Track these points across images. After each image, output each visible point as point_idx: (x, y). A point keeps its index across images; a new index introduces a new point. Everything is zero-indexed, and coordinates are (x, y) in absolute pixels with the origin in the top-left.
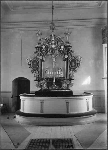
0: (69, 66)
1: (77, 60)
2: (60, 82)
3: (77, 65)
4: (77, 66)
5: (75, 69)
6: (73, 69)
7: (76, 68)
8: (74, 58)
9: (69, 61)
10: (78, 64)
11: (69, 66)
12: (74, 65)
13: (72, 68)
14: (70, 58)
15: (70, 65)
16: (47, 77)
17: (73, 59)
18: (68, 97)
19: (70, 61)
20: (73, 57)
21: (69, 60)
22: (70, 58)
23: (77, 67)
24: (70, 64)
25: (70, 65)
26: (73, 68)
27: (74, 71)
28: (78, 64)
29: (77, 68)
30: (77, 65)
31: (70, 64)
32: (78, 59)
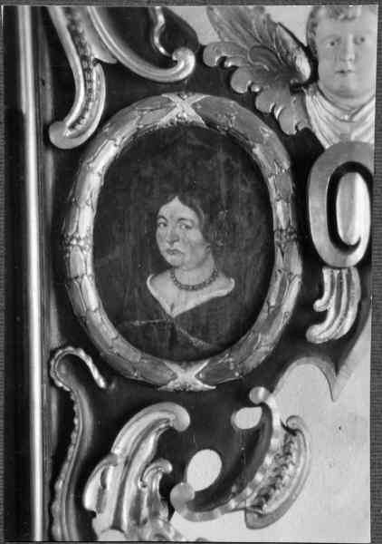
0: (74, 327)
1: (304, 151)
2: (207, 125)
3: (285, 297)
4: (306, 313)
5: (245, 419)
6: (182, 418)
7: (270, 373)
8: (211, 79)
9: (70, 163)
10: (313, 262)
11: (74, 327)
13: (148, 395)
14: (91, 98)
15: (90, 297)
16: (201, 252)
17: (184, 109)
18: (72, 463)
19: (93, 180)
20: (186, 64)
21: (64, 136)
22: (91, 98)
23: (294, 342)
24: (82, 260)
25: (90, 297)
26: (190, 377)
27: (204, 468)
28: (313, 262)
29: (303, 376)
30: (285, 297)
31: (82, 260)
32: (321, 116)
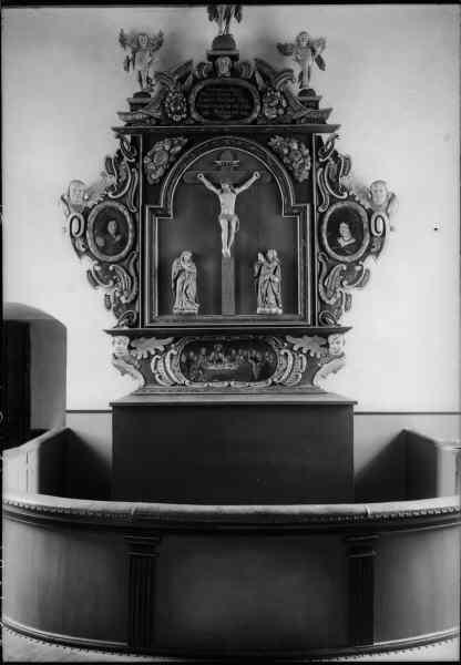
7: (363, 258)
9: (322, 215)
10: (372, 235)
12: (353, 241)
19: (326, 220)
20: (346, 195)
21: (321, 210)
23: (368, 252)
